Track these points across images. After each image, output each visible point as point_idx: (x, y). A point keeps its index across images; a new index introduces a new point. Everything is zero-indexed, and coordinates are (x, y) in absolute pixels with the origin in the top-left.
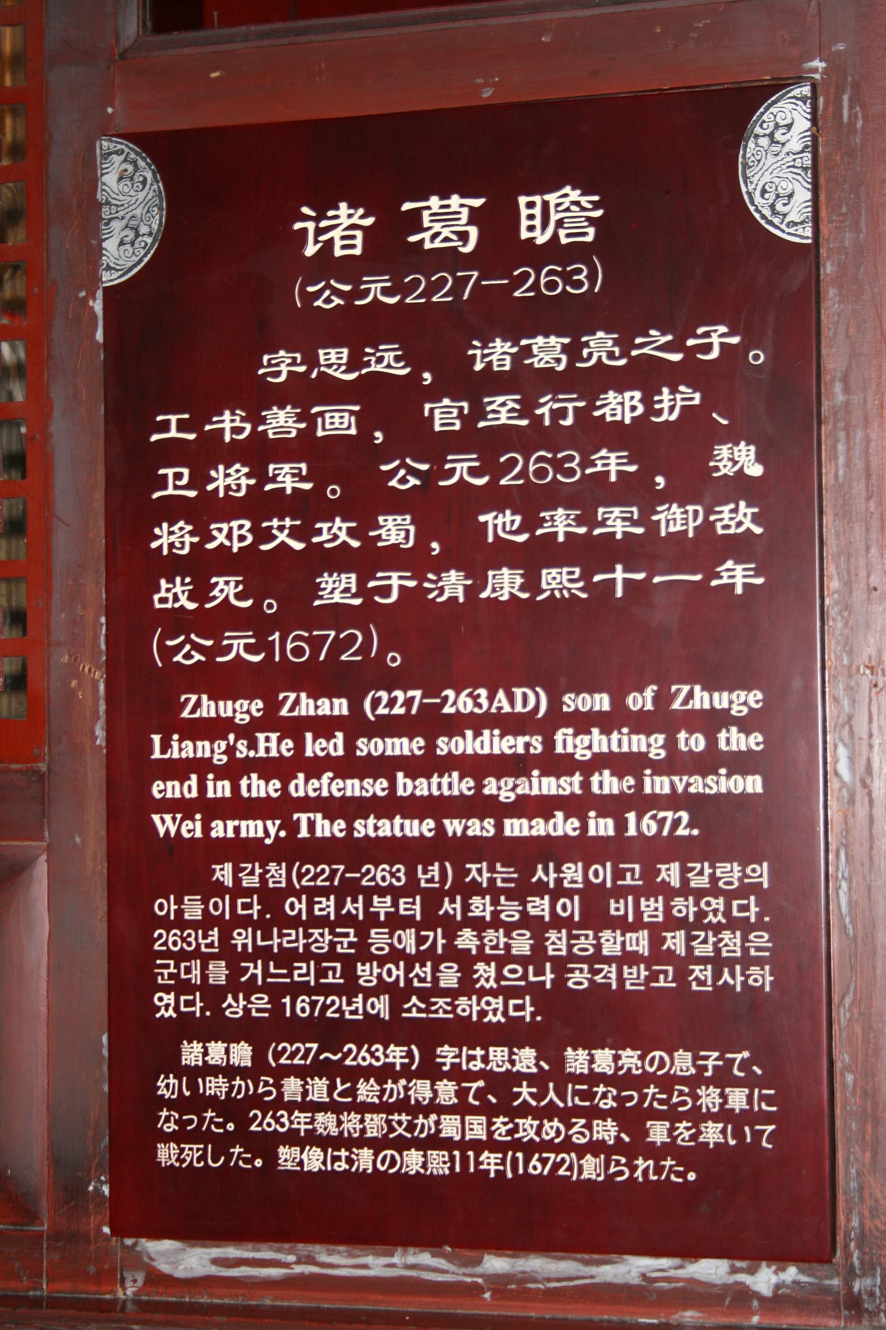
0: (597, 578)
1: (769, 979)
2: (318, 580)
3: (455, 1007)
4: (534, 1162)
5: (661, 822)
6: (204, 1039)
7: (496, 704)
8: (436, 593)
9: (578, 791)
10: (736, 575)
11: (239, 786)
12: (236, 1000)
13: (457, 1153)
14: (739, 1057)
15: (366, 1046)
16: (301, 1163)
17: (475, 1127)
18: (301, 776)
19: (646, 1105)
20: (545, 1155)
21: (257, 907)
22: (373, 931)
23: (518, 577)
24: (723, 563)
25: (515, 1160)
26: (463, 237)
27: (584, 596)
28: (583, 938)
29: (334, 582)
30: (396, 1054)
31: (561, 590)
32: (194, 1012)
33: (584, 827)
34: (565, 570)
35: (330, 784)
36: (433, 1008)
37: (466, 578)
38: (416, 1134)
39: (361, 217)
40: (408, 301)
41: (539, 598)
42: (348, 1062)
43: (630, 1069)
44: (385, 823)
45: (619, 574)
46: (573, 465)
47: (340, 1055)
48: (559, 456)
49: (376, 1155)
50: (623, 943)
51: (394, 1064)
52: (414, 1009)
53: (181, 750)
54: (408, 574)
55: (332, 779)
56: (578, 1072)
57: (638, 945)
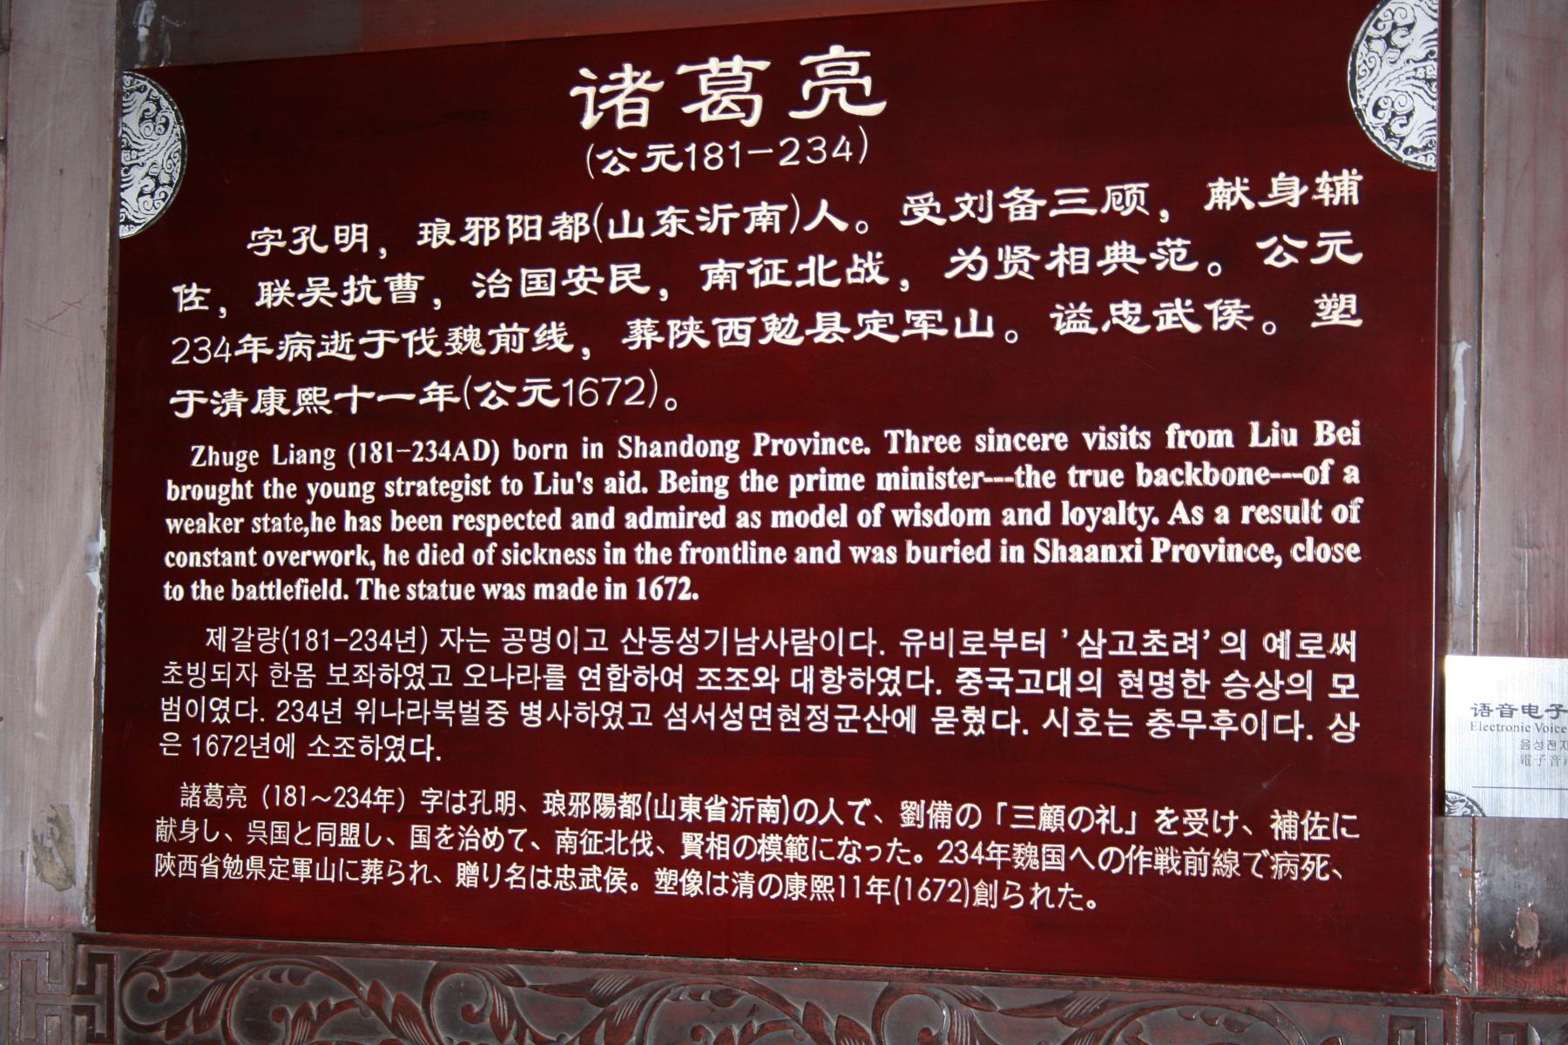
0: (338, 397)
3: (357, 745)
13: (842, 877)
14: (861, 804)
16: (679, 888)
17: (1053, 856)
24: (428, 384)
25: (903, 884)
27: (329, 412)
32: (1292, 735)
39: (648, 81)
44: (433, 588)
45: (355, 394)
49: (757, 879)
50: (631, 680)
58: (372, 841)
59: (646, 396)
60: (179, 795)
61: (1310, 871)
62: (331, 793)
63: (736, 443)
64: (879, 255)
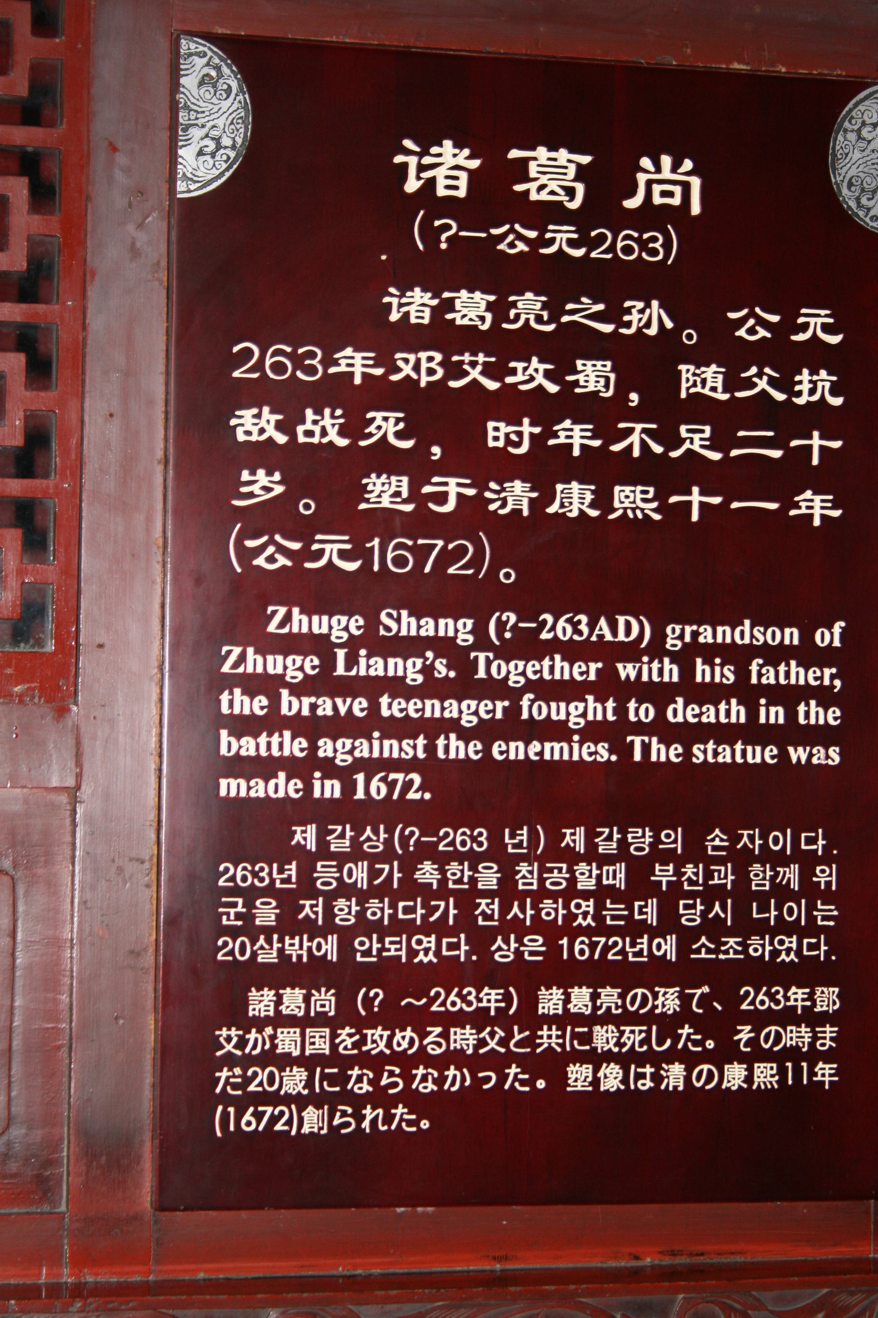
0: (673, 499)
1: (452, 912)
2: (364, 481)
3: (746, 947)
4: (247, 1117)
5: (392, 785)
6: (566, 984)
7: (597, 632)
8: (498, 503)
9: (611, 717)
10: (815, 506)
11: (796, 713)
12: (507, 941)
14: (699, 992)
15: (456, 990)
17: (317, 1040)
18: (680, 700)
19: (680, 1046)
20: (260, 1109)
21: (821, 842)
22: (319, 864)
23: (588, 493)
26: (570, 192)
28: (556, 871)
29: (383, 484)
30: (491, 998)
31: (634, 510)
33: (308, 788)
34: (639, 488)
35: (530, 707)
36: (723, 948)
37: (532, 490)
38: (247, 1051)
40: (593, 255)
41: (611, 517)
42: (434, 1008)
43: (609, 1009)
45: (696, 497)
46: (314, 362)
47: (424, 1000)
48: (300, 351)
50: (599, 878)
51: (489, 1008)
52: (703, 950)
53: (369, 667)
54: (468, 481)
55: (533, 702)
56: (263, 1014)
57: (614, 878)
58: (660, 1043)
59: (476, 562)
60: (246, 1003)
61: (629, 1044)
62: (428, 996)
63: (470, 623)
64: (339, 412)
